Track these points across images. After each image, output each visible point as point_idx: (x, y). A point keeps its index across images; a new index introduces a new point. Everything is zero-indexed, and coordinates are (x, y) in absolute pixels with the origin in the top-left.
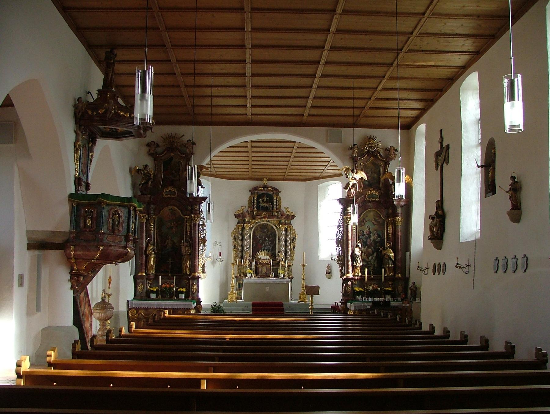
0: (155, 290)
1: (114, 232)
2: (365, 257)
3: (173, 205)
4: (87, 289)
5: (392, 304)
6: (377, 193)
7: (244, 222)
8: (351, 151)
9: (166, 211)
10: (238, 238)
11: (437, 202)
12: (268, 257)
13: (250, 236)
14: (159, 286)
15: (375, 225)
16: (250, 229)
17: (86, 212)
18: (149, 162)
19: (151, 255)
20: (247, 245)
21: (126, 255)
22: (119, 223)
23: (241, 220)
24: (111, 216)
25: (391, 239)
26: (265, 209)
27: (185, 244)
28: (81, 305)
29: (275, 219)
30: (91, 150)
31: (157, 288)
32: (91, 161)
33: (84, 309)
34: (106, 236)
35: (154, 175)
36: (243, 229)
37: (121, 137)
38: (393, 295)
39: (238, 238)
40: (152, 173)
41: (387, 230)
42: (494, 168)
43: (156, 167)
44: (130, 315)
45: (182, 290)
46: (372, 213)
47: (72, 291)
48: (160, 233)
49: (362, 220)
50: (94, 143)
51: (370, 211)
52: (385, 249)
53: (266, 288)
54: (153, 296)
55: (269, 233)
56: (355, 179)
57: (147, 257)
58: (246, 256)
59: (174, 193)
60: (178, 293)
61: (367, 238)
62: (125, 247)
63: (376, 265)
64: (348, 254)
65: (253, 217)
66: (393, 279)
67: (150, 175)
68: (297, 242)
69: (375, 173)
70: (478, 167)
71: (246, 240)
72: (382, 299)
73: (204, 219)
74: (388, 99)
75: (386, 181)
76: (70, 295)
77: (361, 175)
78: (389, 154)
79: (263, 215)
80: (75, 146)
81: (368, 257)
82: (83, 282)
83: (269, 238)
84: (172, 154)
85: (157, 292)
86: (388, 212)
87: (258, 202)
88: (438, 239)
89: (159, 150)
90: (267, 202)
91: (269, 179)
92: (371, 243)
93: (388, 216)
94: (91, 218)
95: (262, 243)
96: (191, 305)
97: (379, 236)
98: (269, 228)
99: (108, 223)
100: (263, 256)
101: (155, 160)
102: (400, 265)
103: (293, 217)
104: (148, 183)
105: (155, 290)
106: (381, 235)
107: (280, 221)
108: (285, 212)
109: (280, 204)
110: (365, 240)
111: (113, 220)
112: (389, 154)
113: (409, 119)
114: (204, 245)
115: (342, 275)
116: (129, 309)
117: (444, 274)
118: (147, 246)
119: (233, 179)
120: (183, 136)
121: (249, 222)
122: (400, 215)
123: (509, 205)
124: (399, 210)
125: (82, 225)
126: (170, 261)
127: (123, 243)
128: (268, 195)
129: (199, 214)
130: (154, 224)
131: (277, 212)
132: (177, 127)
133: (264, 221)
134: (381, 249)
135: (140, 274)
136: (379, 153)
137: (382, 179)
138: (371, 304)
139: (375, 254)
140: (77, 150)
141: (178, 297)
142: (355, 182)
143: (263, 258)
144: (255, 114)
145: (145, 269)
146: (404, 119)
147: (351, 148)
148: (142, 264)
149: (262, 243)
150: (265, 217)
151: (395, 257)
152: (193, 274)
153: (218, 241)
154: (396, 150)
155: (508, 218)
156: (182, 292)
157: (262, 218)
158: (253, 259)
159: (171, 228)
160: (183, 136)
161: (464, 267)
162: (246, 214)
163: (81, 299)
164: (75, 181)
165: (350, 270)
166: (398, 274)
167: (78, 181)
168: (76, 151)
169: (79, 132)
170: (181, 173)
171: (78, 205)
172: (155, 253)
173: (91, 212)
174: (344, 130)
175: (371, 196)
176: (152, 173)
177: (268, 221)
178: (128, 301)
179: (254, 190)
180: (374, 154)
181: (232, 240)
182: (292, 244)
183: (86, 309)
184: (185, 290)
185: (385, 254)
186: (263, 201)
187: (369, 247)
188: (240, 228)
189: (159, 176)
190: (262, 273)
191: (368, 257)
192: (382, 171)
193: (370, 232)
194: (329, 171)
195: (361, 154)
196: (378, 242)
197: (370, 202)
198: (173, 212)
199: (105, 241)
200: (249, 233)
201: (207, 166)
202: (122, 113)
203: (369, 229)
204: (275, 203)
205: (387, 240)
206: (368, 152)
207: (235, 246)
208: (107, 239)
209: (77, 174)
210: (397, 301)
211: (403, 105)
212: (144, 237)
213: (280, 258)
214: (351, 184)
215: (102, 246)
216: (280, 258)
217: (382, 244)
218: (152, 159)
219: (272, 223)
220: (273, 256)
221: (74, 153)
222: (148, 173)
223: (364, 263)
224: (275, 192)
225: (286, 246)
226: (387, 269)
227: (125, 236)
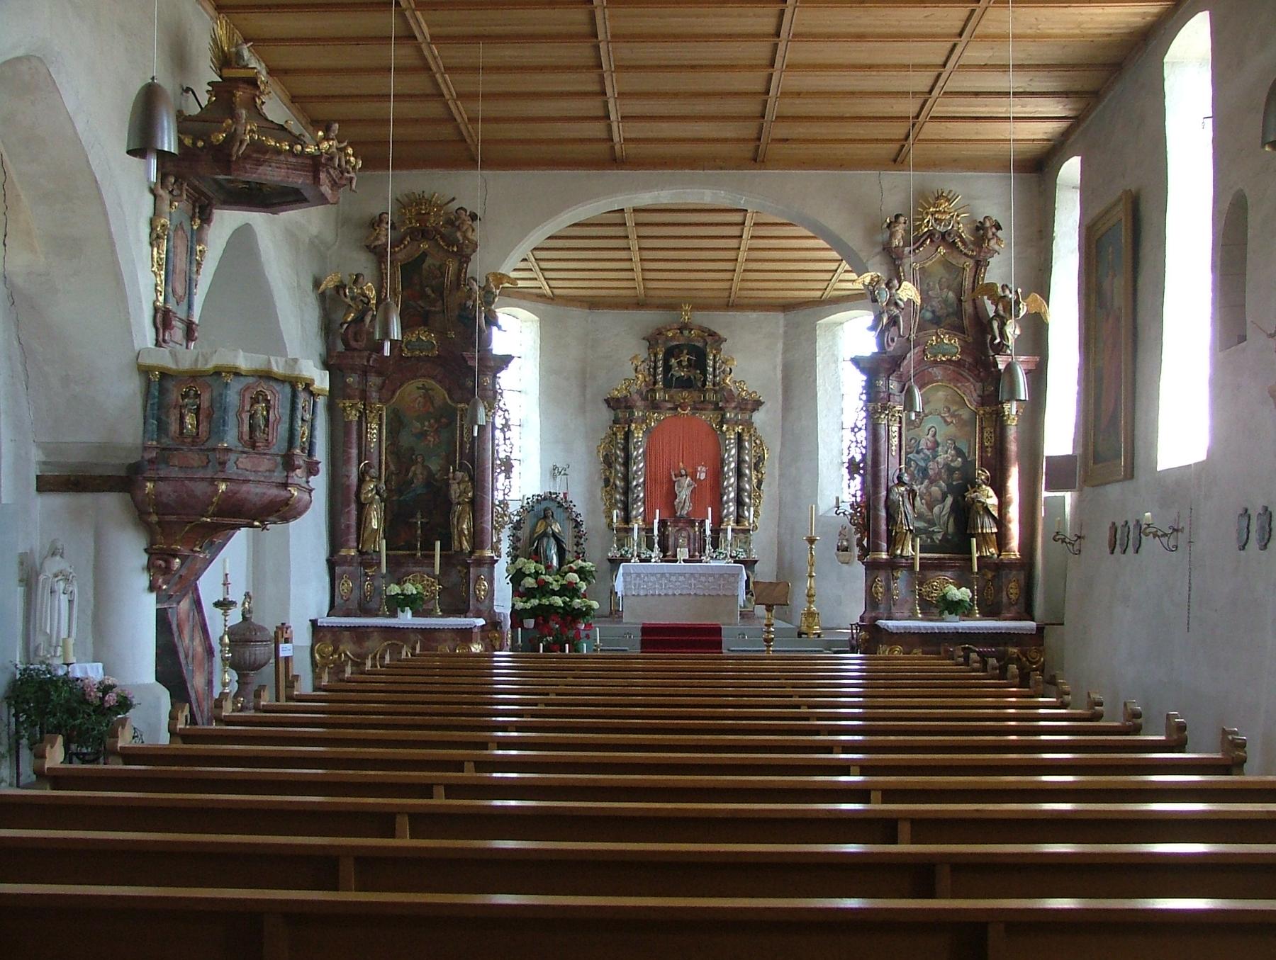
1: (254, 447)
4: (196, 589)
17: (184, 396)
19: (371, 503)
21: (287, 504)
22: (267, 425)
24: (247, 407)
26: (686, 384)
27: (459, 474)
28: (180, 632)
30: (198, 237)
32: (199, 264)
33: (188, 643)
34: (233, 457)
36: (628, 435)
37: (273, 205)
41: (982, 438)
44: (317, 657)
46: (941, 394)
47: (154, 596)
48: (395, 450)
50: (206, 219)
51: (937, 389)
62: (285, 485)
65: (655, 406)
69: (949, 288)
74: (977, 94)
75: (463, 307)
76: (148, 605)
80: (153, 229)
82: (183, 572)
84: (424, 246)
87: (668, 369)
91: (697, 307)
92: (939, 474)
94: (197, 412)
97: (959, 452)
99: (240, 424)
106: (965, 451)
107: (723, 416)
108: (735, 392)
110: (922, 464)
111: (251, 417)
113: (1038, 145)
115: (864, 552)
117: (1264, 547)
121: (644, 420)
127: (278, 476)
128: (693, 350)
129: (495, 398)
130: (380, 426)
132: (438, 173)
135: (343, 552)
136: (960, 237)
139: (949, 500)
140: (158, 237)
144: (632, 140)
146: (1023, 146)
148: (348, 527)
159: (423, 435)
160: (454, 199)
161: (1165, 535)
162: (636, 397)
163: (183, 615)
165: (884, 545)
168: (155, 240)
169: (161, 192)
183: (197, 642)
186: (680, 363)
187: (932, 482)
188: (620, 436)
191: (931, 509)
194: (844, 285)
196: (958, 469)
199: (231, 469)
201: (513, 275)
203: (934, 436)
206: (931, 234)
207: (607, 481)
208: (240, 464)
209: (161, 298)
211: (1018, 109)
212: (354, 460)
215: (224, 480)
221: (151, 245)
227: (283, 456)
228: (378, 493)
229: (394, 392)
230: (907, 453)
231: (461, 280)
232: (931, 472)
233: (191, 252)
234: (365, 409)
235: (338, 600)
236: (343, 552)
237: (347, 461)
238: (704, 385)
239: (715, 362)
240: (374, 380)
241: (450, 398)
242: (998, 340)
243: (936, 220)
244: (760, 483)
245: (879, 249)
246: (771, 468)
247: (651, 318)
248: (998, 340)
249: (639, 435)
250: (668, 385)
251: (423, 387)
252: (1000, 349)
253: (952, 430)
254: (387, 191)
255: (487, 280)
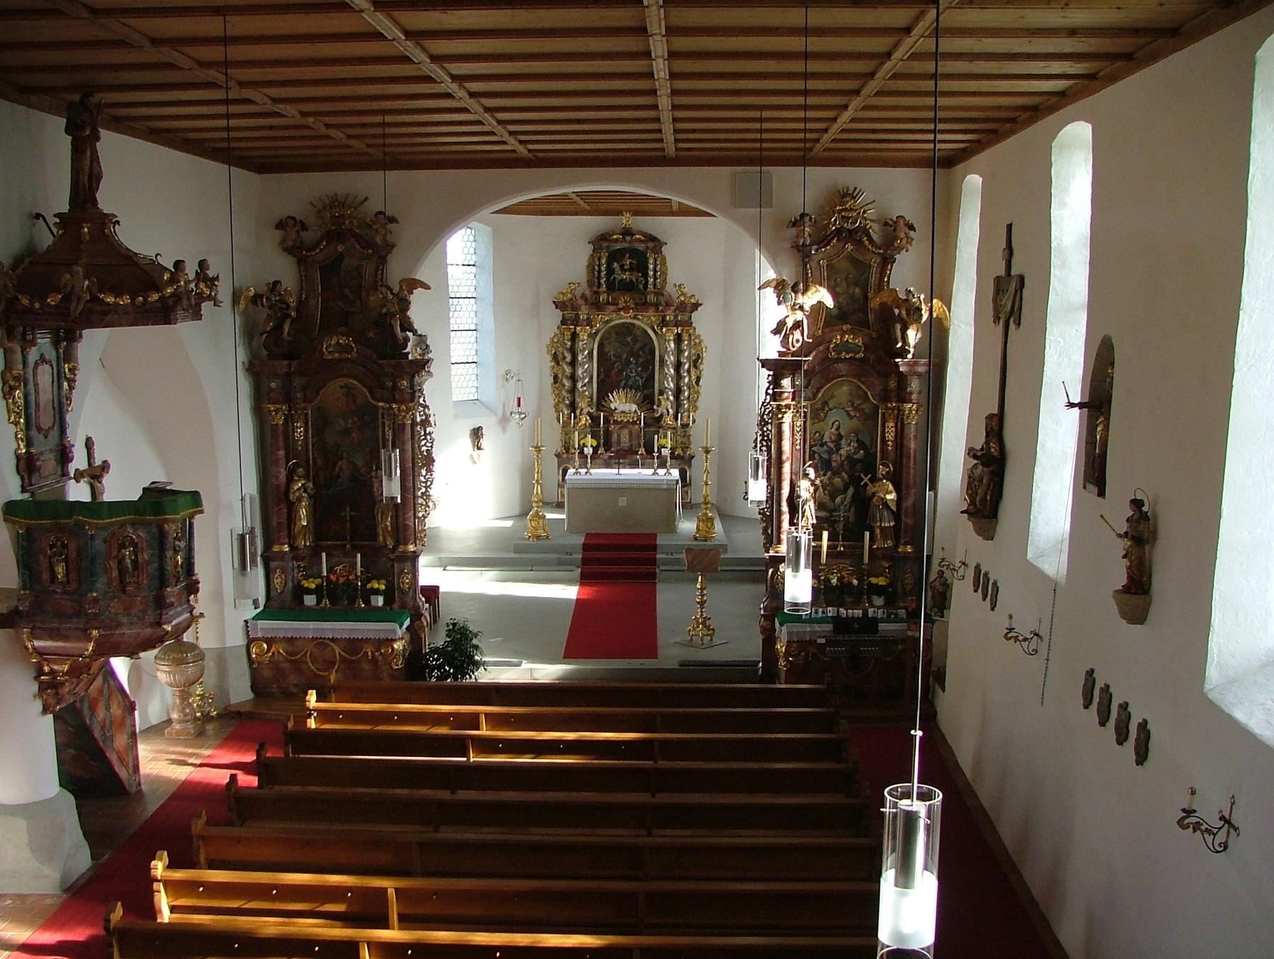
0: (313, 586)
1: (124, 591)
2: (826, 499)
3: (351, 377)
5: (882, 626)
6: (859, 341)
7: (576, 322)
8: (794, 231)
9: (334, 392)
10: (564, 356)
11: (990, 418)
12: (634, 407)
13: (591, 353)
14: (322, 577)
15: (852, 418)
16: (592, 336)
18: (285, 271)
20: (584, 378)
23: (569, 314)
25: (892, 455)
26: (628, 287)
29: (651, 312)
31: (318, 581)
35: (300, 302)
36: (574, 336)
38: (891, 596)
39: (564, 358)
40: (292, 301)
42: (1108, 419)
43: (304, 278)
45: (376, 586)
49: (819, 406)
51: (841, 384)
52: (874, 480)
53: (620, 499)
54: (310, 600)
55: (638, 345)
56: (801, 308)
57: (292, 509)
58: (582, 404)
59: (348, 349)
60: (367, 594)
61: (830, 452)
63: (851, 519)
64: (780, 495)
65: (597, 306)
66: (891, 556)
67: (288, 306)
68: (707, 366)
70: (1071, 405)
71: (582, 365)
72: (858, 613)
73: (426, 407)
77: (821, 295)
78: (894, 234)
79: (621, 305)
81: (833, 498)
83: (637, 357)
84: (340, 248)
85: (317, 591)
86: (887, 386)
87: (610, 271)
88: (984, 517)
89: (309, 237)
90: (631, 270)
91: (636, 213)
92: (842, 465)
93: (885, 398)
94: (66, 561)
95: (621, 371)
96: (394, 631)
97: (861, 445)
98: (638, 332)
99: (107, 571)
100: (623, 404)
101: (299, 264)
102: (910, 522)
103: (696, 306)
104: (281, 327)
105: (313, 586)
107: (664, 317)
108: (675, 296)
109: (664, 273)
110: (825, 456)
112: (894, 234)
114: (429, 471)
116: (250, 641)
118: (290, 480)
119: (549, 213)
120: (366, 199)
121: (589, 323)
122: (914, 396)
123: (1119, 576)
124: (914, 385)
125: (46, 576)
126: (348, 513)
128: (634, 253)
131: (656, 294)
132: (351, 174)
133: (625, 318)
134: (866, 480)
135: (276, 548)
137: (875, 303)
138: (829, 627)
139: (851, 491)
141: (367, 602)
142: (799, 316)
143: (620, 409)
145: (289, 537)
147: (795, 224)
149: (621, 371)
150: (626, 309)
151: (899, 501)
152: (401, 548)
153: (514, 370)
154: (911, 228)
155: (1114, 609)
156: (377, 592)
157: (620, 310)
158: (598, 410)
159: (347, 432)
160: (366, 199)
161: (1025, 639)
162: (580, 302)
164: (17, 466)
166: (906, 544)
167: (27, 466)
170: (364, 294)
171: (29, 530)
172: (310, 497)
173: (64, 546)
174: (778, 172)
175: (845, 346)
176: (292, 301)
177: (635, 317)
178: (246, 622)
179: (600, 241)
180: (855, 235)
181: (548, 362)
182: (693, 370)
184: (383, 587)
185: (874, 494)
186: (622, 267)
187: (835, 474)
188: (568, 335)
189: (312, 302)
190: (619, 442)
191: (833, 498)
192: (873, 280)
193: (840, 437)
195: (822, 241)
196: (858, 460)
197: (839, 360)
198: (350, 393)
200: (588, 346)
202: (110, 300)
203: (838, 429)
204: (651, 273)
205: (882, 458)
206: (838, 232)
207: (556, 378)
210: (897, 620)
212: (283, 461)
213: (661, 410)
214: (790, 323)
216: (661, 410)
217: (870, 468)
218: (294, 260)
219: (645, 321)
220: (648, 401)
221: (4, 397)
222: (283, 301)
223: (823, 514)
224: (650, 245)
225: (679, 377)
226: (878, 531)
228: (305, 491)
229: (317, 393)
230: (811, 446)
231: (379, 281)
232: (834, 464)
233: (59, 377)
234: (290, 410)
235: (273, 594)
236: (276, 548)
237: (276, 462)
238: (646, 287)
239: (656, 265)
240: (298, 382)
241: (373, 398)
242: (899, 345)
243: (843, 217)
244: (698, 379)
245: (787, 245)
246: (708, 367)
247: (597, 223)
248: (899, 345)
249: (584, 336)
250: (611, 287)
251: (346, 386)
252: (903, 353)
253: (855, 422)
254: (300, 192)
255: (401, 287)
